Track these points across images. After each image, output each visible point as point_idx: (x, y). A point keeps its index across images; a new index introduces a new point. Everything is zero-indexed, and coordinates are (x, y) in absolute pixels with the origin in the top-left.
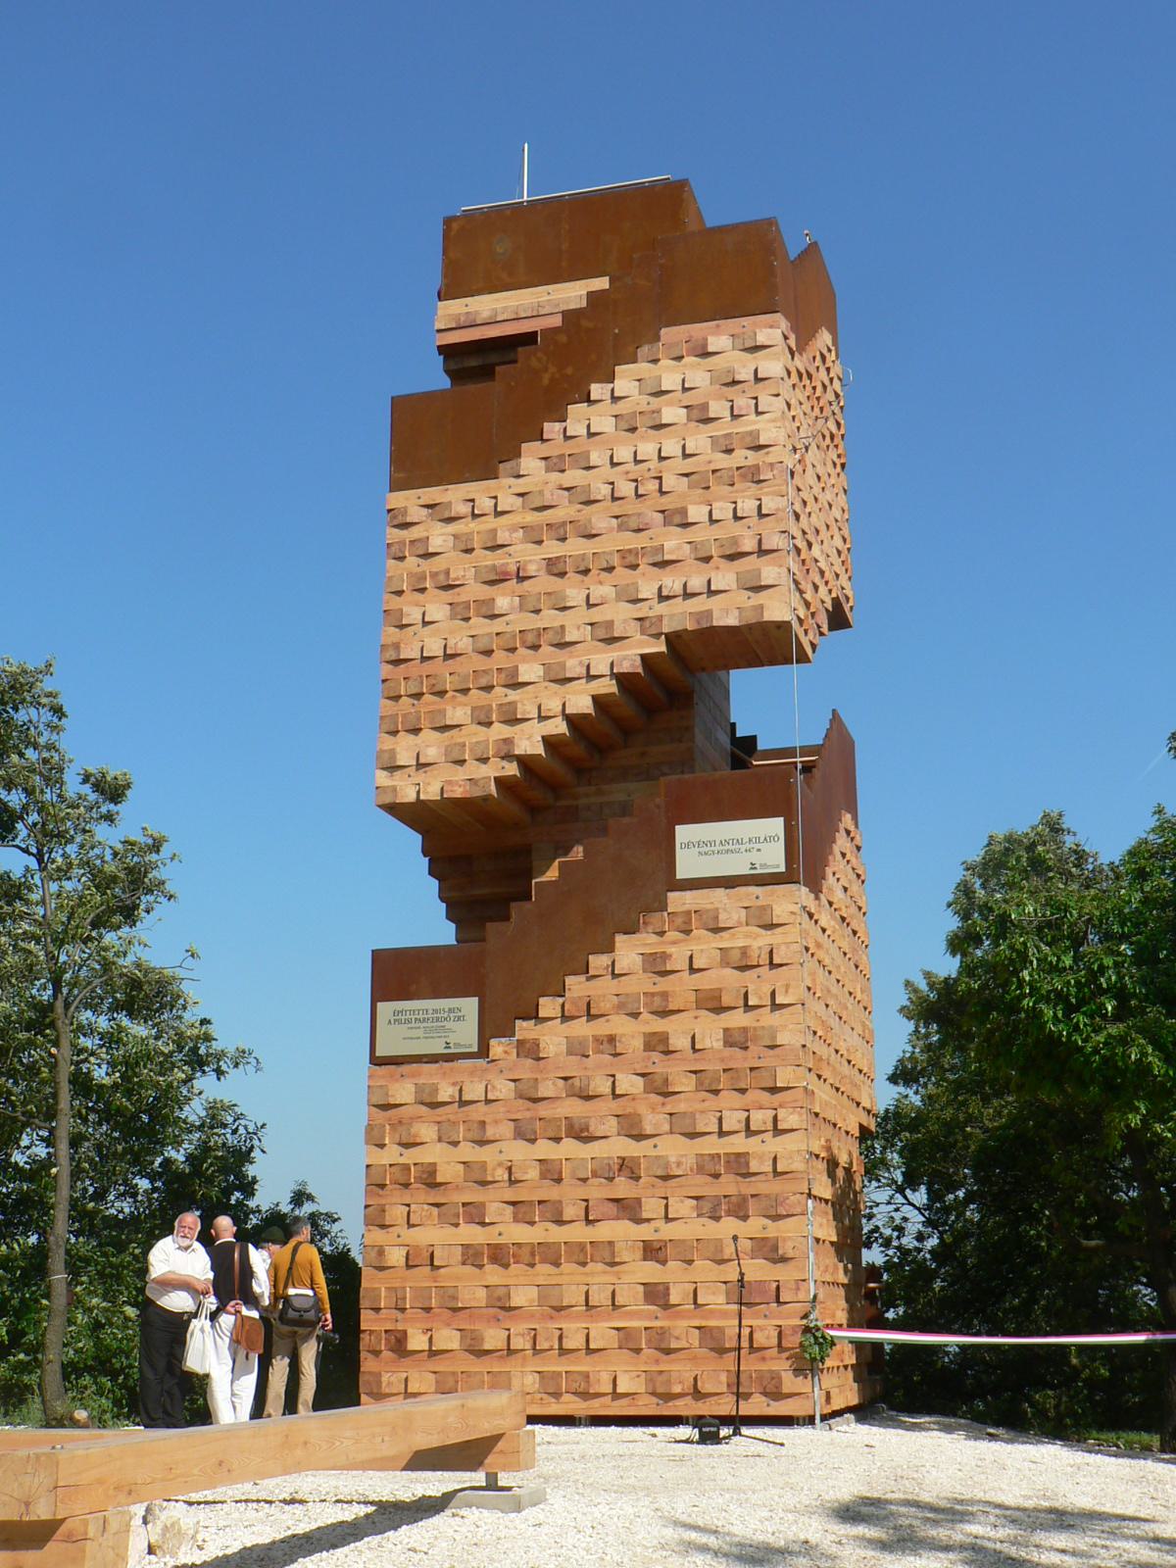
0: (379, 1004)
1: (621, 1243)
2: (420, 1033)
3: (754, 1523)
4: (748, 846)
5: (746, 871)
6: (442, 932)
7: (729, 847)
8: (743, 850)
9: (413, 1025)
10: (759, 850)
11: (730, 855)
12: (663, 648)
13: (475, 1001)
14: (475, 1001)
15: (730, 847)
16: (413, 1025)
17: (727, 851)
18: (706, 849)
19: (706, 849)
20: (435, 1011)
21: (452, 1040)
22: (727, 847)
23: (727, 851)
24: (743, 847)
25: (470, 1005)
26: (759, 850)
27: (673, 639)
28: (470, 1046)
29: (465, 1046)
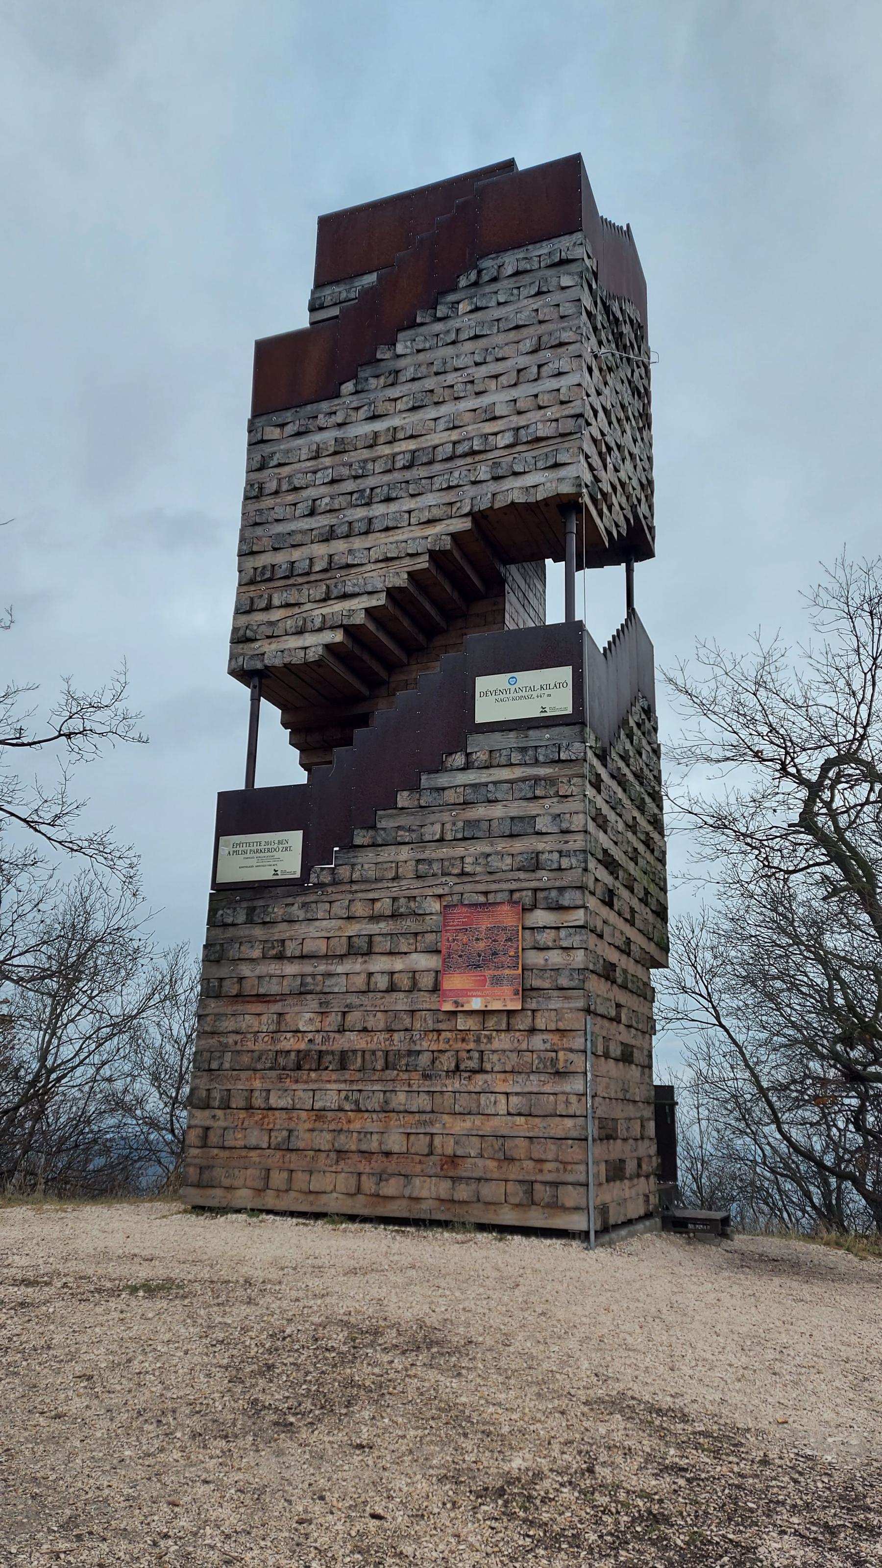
0: (479, 719)
1: (511, 1105)
2: (254, 862)
3: (395, 1247)
4: (539, 692)
5: (536, 714)
6: (624, 565)
7: (527, 693)
8: (535, 696)
9: (248, 855)
10: (549, 695)
11: (524, 701)
12: (382, 602)
13: (300, 833)
14: (300, 833)
15: (524, 694)
16: (248, 855)
17: (520, 698)
18: (502, 696)
19: (502, 696)
20: (267, 843)
21: (279, 869)
22: (521, 694)
23: (520, 698)
24: (535, 694)
25: (296, 838)
26: (549, 695)
27: (477, 517)
28: (295, 873)
29: (290, 873)
